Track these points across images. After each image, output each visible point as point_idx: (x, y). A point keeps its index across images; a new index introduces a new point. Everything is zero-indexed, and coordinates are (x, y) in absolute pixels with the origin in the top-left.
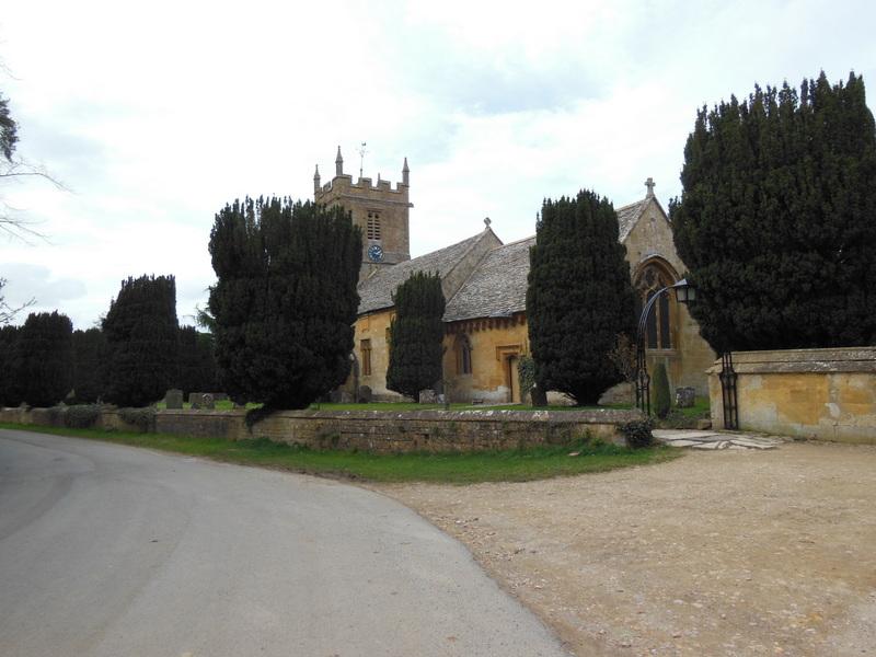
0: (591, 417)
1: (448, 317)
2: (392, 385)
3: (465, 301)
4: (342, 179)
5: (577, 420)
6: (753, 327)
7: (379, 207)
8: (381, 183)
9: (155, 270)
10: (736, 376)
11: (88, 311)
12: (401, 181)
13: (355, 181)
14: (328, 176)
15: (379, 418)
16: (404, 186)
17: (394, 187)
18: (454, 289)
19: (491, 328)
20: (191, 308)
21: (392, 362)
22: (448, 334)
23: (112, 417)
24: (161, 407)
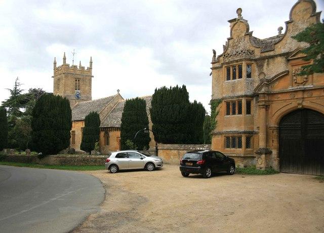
1: (101, 126)
3: (105, 122)
4: (65, 65)
7: (79, 77)
12: (89, 66)
14: (60, 63)
16: (90, 69)
17: (86, 69)
18: (105, 115)
21: (83, 141)
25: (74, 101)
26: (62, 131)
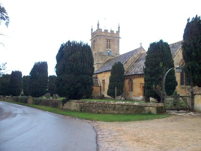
0: (148, 105)
2: (109, 94)
4: (99, 30)
5: (145, 105)
8: (111, 31)
9: (41, 60)
11: (26, 72)
12: (117, 30)
13: (103, 31)
14: (95, 29)
15: (96, 103)
16: (118, 32)
19: (139, 77)
20: (52, 71)
23: (30, 99)
24: (44, 98)
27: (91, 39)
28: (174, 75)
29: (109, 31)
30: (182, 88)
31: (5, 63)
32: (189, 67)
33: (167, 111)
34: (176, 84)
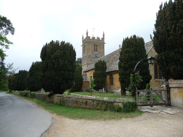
0: (117, 100)
1: (107, 71)
4: (88, 37)
6: (175, 72)
10: (170, 88)
12: (102, 37)
13: (91, 38)
14: (85, 37)
16: (103, 39)
17: (101, 39)
22: (108, 75)
25: (94, 58)
26: (63, 72)
27: (82, 45)
28: (148, 68)
29: (96, 38)
30: (157, 81)
31: (11, 64)
32: (162, 58)
33: (138, 107)
34: (151, 77)
